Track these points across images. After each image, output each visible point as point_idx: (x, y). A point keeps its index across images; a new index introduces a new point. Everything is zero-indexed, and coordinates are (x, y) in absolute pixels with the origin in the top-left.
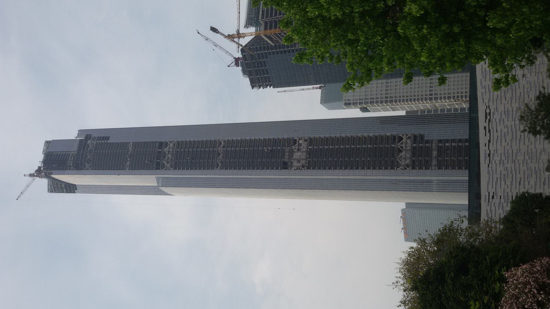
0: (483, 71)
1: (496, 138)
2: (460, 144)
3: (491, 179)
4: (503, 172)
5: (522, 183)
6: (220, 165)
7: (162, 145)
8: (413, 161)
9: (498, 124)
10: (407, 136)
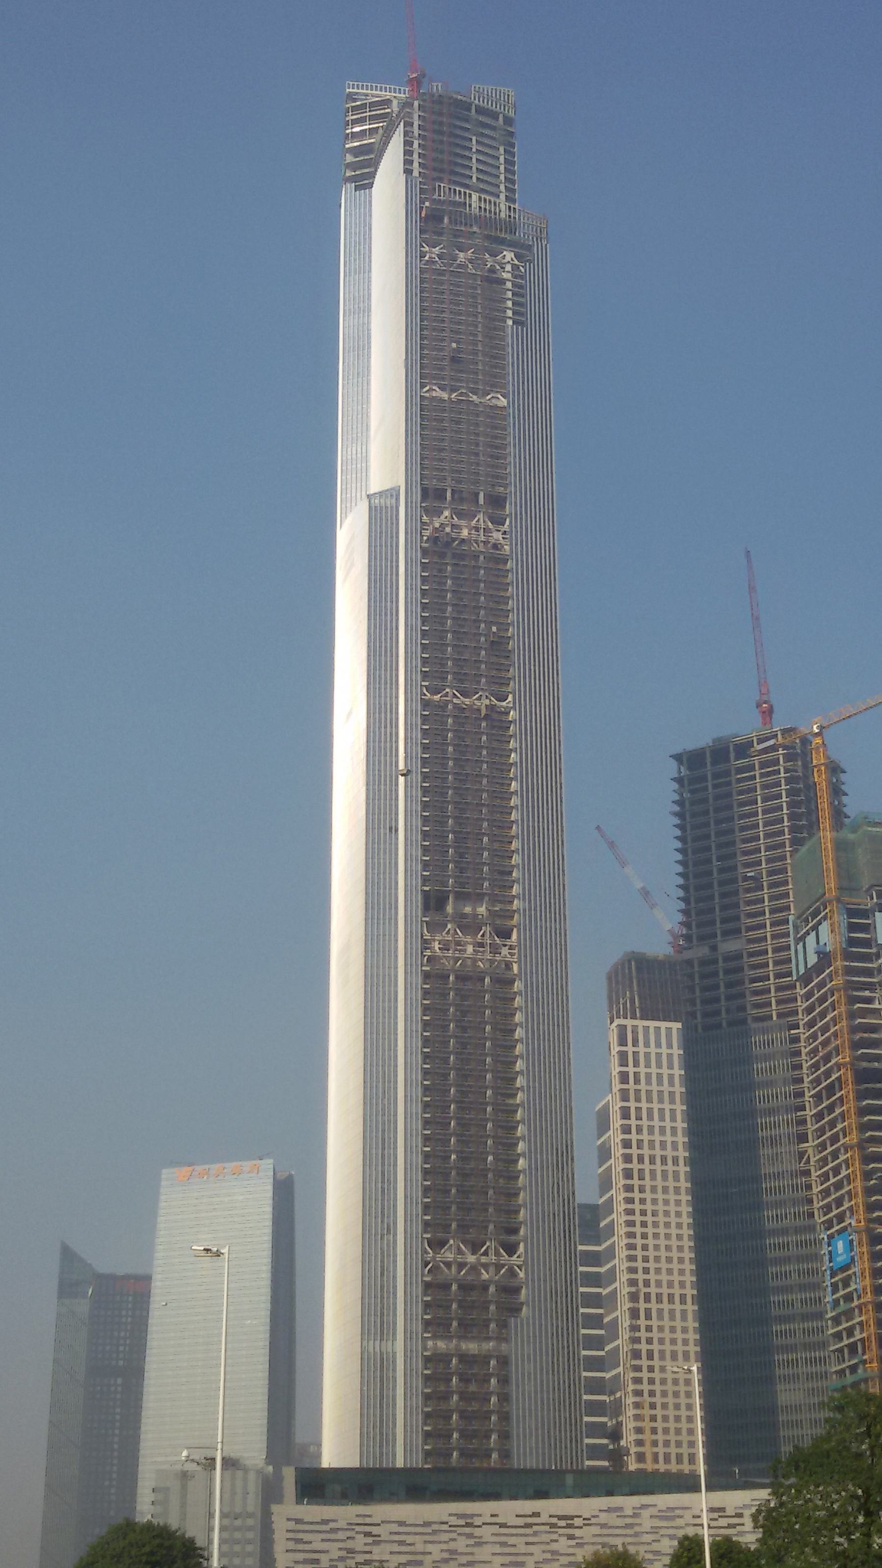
0: (678, 1512)
2: (494, 1399)
3: (514, 1531)
6: (437, 697)
9: (544, 1547)
10: (519, 1267)
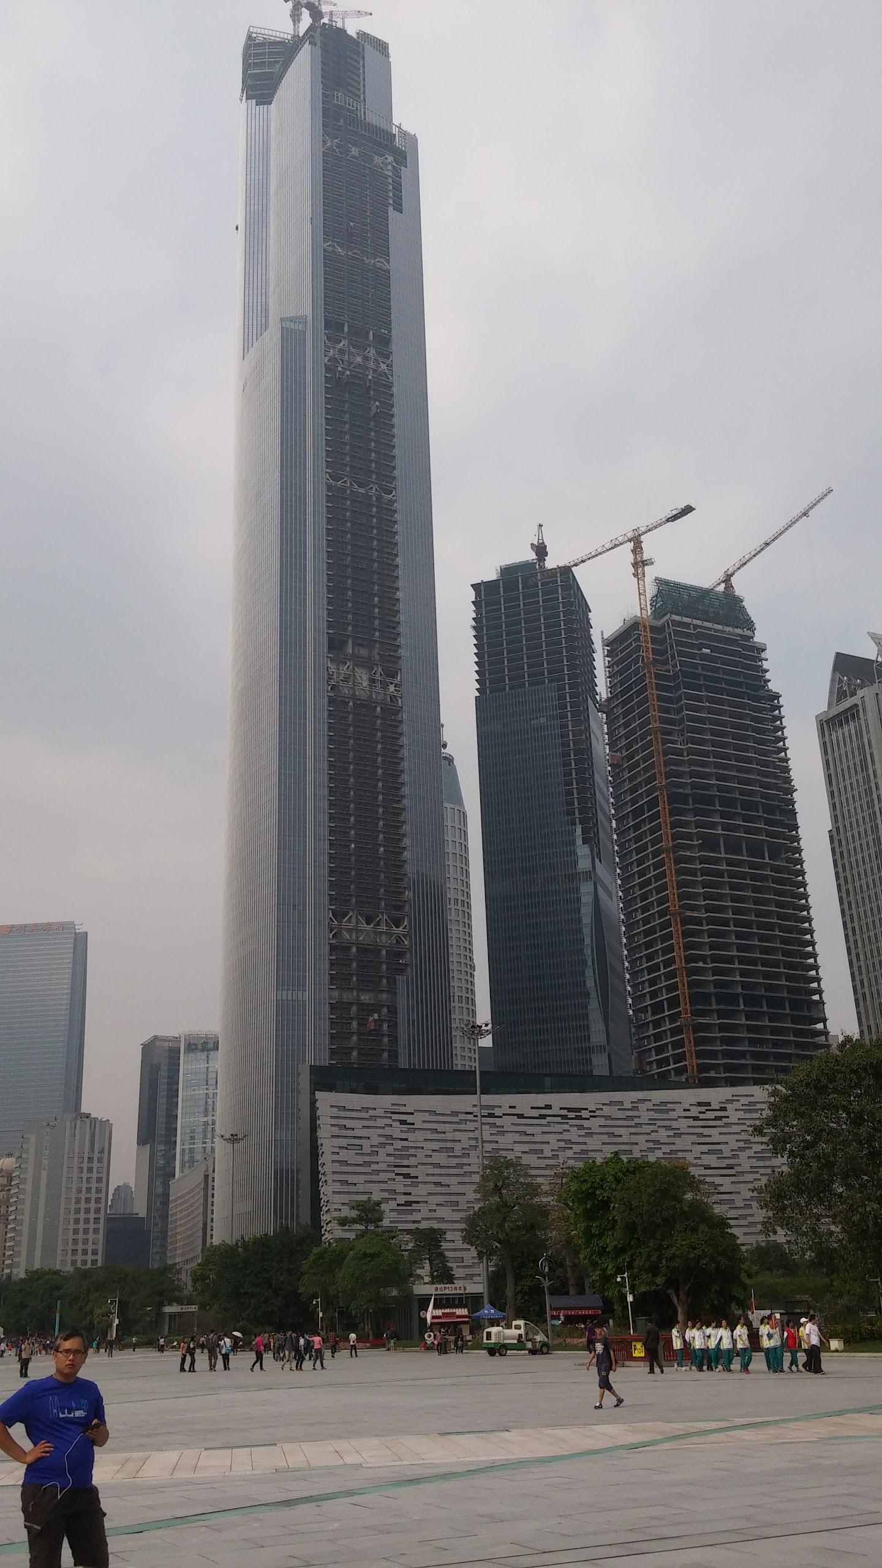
0: (670, 1106)
1: (529, 1130)
4: (458, 1147)
5: (439, 1189)
7: (383, 342)
8: (349, 949)
10: (404, 936)
